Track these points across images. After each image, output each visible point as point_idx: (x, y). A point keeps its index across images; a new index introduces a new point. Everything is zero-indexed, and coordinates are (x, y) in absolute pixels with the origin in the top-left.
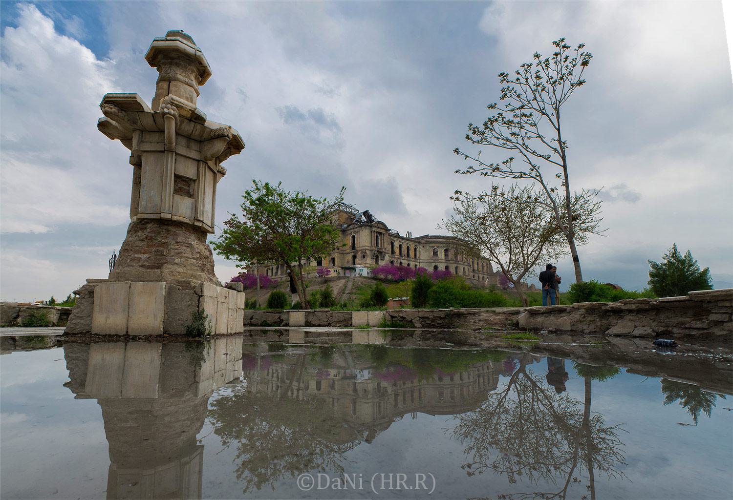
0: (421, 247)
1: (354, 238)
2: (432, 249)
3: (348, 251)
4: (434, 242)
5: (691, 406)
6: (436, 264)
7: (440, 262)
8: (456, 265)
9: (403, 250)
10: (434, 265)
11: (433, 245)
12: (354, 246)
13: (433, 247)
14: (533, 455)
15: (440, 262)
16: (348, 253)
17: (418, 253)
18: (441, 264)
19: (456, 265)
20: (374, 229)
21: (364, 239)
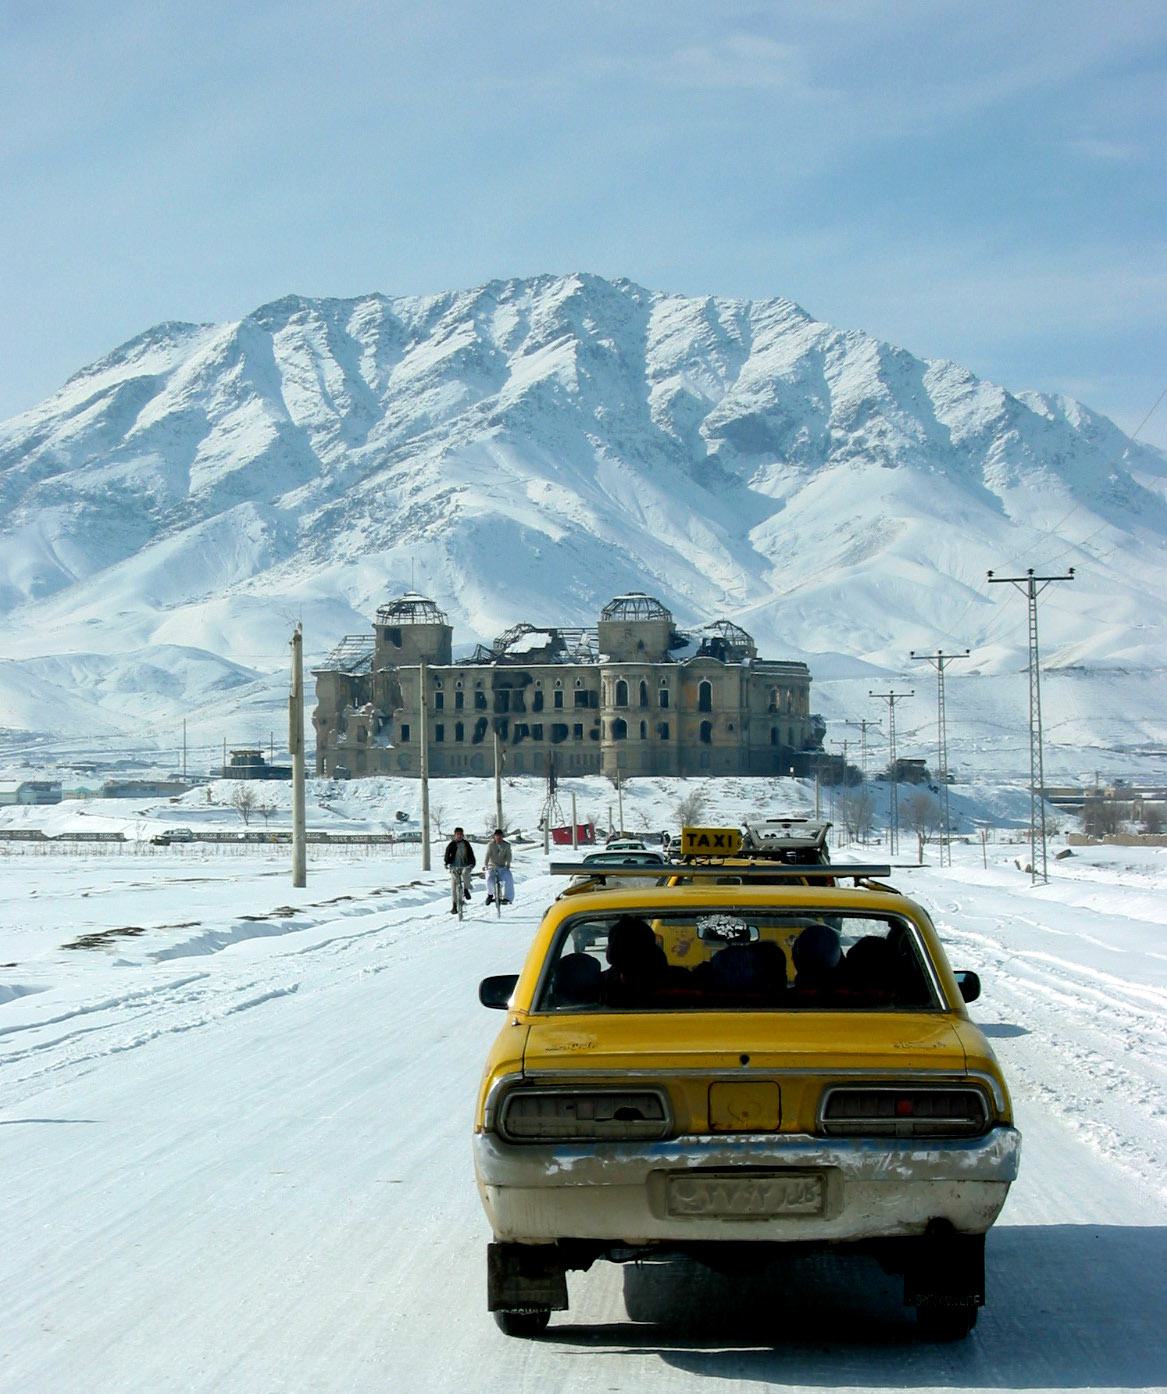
1: (705, 688)
12: (705, 705)
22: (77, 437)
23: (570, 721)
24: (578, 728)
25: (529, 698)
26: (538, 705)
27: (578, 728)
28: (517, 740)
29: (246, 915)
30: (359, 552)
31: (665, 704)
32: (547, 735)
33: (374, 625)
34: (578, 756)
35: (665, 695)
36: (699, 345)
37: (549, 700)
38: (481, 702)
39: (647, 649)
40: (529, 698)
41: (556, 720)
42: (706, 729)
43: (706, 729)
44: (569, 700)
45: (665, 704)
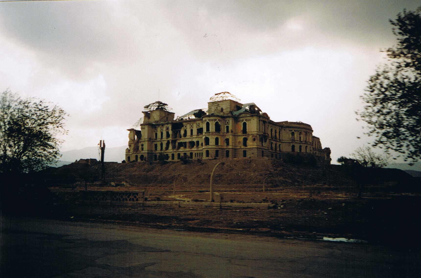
0: (283, 130)
1: (245, 124)
2: (290, 132)
3: (240, 134)
4: (293, 127)
5: (23, 140)
6: (294, 144)
7: (296, 143)
8: (306, 145)
9: (193, 132)
10: (292, 144)
11: (291, 129)
12: (244, 131)
13: (291, 130)
14: (19, 151)
15: (296, 143)
16: (239, 136)
17: (281, 135)
18: (297, 144)
19: (306, 145)
20: (261, 119)
21: (253, 126)
22: (239, 238)
23: (195, 140)
24: (198, 142)
25: (182, 132)
26: (185, 135)
27: (198, 142)
28: (179, 148)
29: (106, 145)
30: (385, 143)
31: (228, 131)
32: (188, 145)
33: (143, 112)
34: (200, 153)
35: (228, 127)
36: (23, 130)
37: (189, 133)
38: (168, 135)
39: (224, 111)
40: (182, 132)
41: (190, 140)
42: (245, 140)
43: (245, 140)
44: (195, 132)
45: (228, 131)
